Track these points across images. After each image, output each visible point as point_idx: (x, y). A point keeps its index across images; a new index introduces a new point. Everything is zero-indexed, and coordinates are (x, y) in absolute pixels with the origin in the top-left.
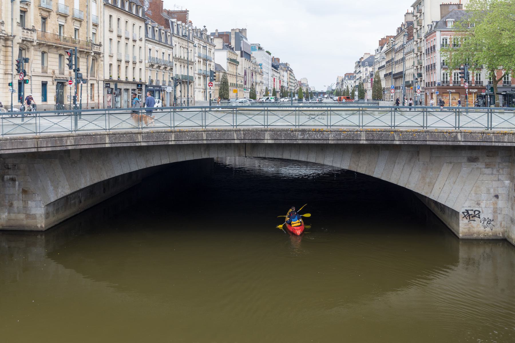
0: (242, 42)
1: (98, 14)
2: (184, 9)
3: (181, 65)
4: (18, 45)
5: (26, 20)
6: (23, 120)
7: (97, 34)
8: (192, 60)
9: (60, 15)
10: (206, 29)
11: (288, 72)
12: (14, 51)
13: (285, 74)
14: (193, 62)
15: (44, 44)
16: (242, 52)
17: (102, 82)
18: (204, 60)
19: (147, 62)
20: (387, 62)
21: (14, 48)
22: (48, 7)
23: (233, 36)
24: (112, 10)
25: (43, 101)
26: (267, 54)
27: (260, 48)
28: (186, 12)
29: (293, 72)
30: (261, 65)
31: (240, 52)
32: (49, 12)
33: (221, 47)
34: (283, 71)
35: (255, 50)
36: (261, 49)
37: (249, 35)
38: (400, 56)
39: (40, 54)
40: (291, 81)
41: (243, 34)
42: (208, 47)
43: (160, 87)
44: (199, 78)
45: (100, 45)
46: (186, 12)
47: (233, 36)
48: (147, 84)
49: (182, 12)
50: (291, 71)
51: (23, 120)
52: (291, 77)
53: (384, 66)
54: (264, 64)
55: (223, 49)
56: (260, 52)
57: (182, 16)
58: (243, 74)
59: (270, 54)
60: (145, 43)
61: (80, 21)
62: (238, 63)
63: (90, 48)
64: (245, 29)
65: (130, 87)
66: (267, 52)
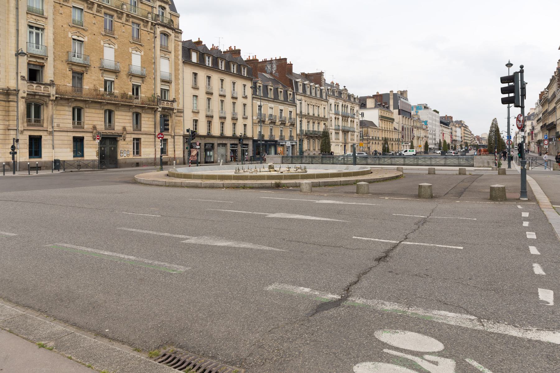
0: (399, 101)
1: (171, 71)
2: (319, 71)
3: (308, 122)
4: (24, 100)
5: (44, 75)
6: (14, 173)
7: (170, 91)
8: (326, 117)
9: (104, 70)
10: (346, 89)
11: (462, 128)
12: (19, 106)
13: (458, 130)
14: (327, 119)
15: (71, 99)
16: (399, 110)
17: (182, 137)
18: (343, 116)
19: (255, 118)
20: (543, 114)
21: (19, 103)
22: (86, 62)
23: (391, 97)
24: (198, 68)
25: (31, 155)
26: (434, 112)
27: (426, 107)
28: (320, 74)
29: (469, 128)
30: (426, 122)
31: (397, 110)
32: (85, 67)
33: (373, 106)
34: (456, 127)
35: (421, 109)
36: (428, 108)
37: (410, 96)
38: (553, 105)
39: (71, 109)
40: (466, 135)
41: (405, 95)
42: (349, 106)
43: (276, 141)
44: (337, 133)
45: (174, 101)
46: (320, 74)
47: (391, 97)
48: (256, 138)
49: (317, 74)
50: (466, 127)
51: (14, 173)
52: (466, 132)
53: (540, 118)
54: (429, 121)
55: (376, 107)
56: (426, 111)
57: (317, 78)
58: (401, 130)
59: (438, 112)
60: (253, 100)
61: (169, 82)
62: (393, 120)
63: (155, 103)
64: (406, 91)
65: (229, 142)
66: (435, 111)
